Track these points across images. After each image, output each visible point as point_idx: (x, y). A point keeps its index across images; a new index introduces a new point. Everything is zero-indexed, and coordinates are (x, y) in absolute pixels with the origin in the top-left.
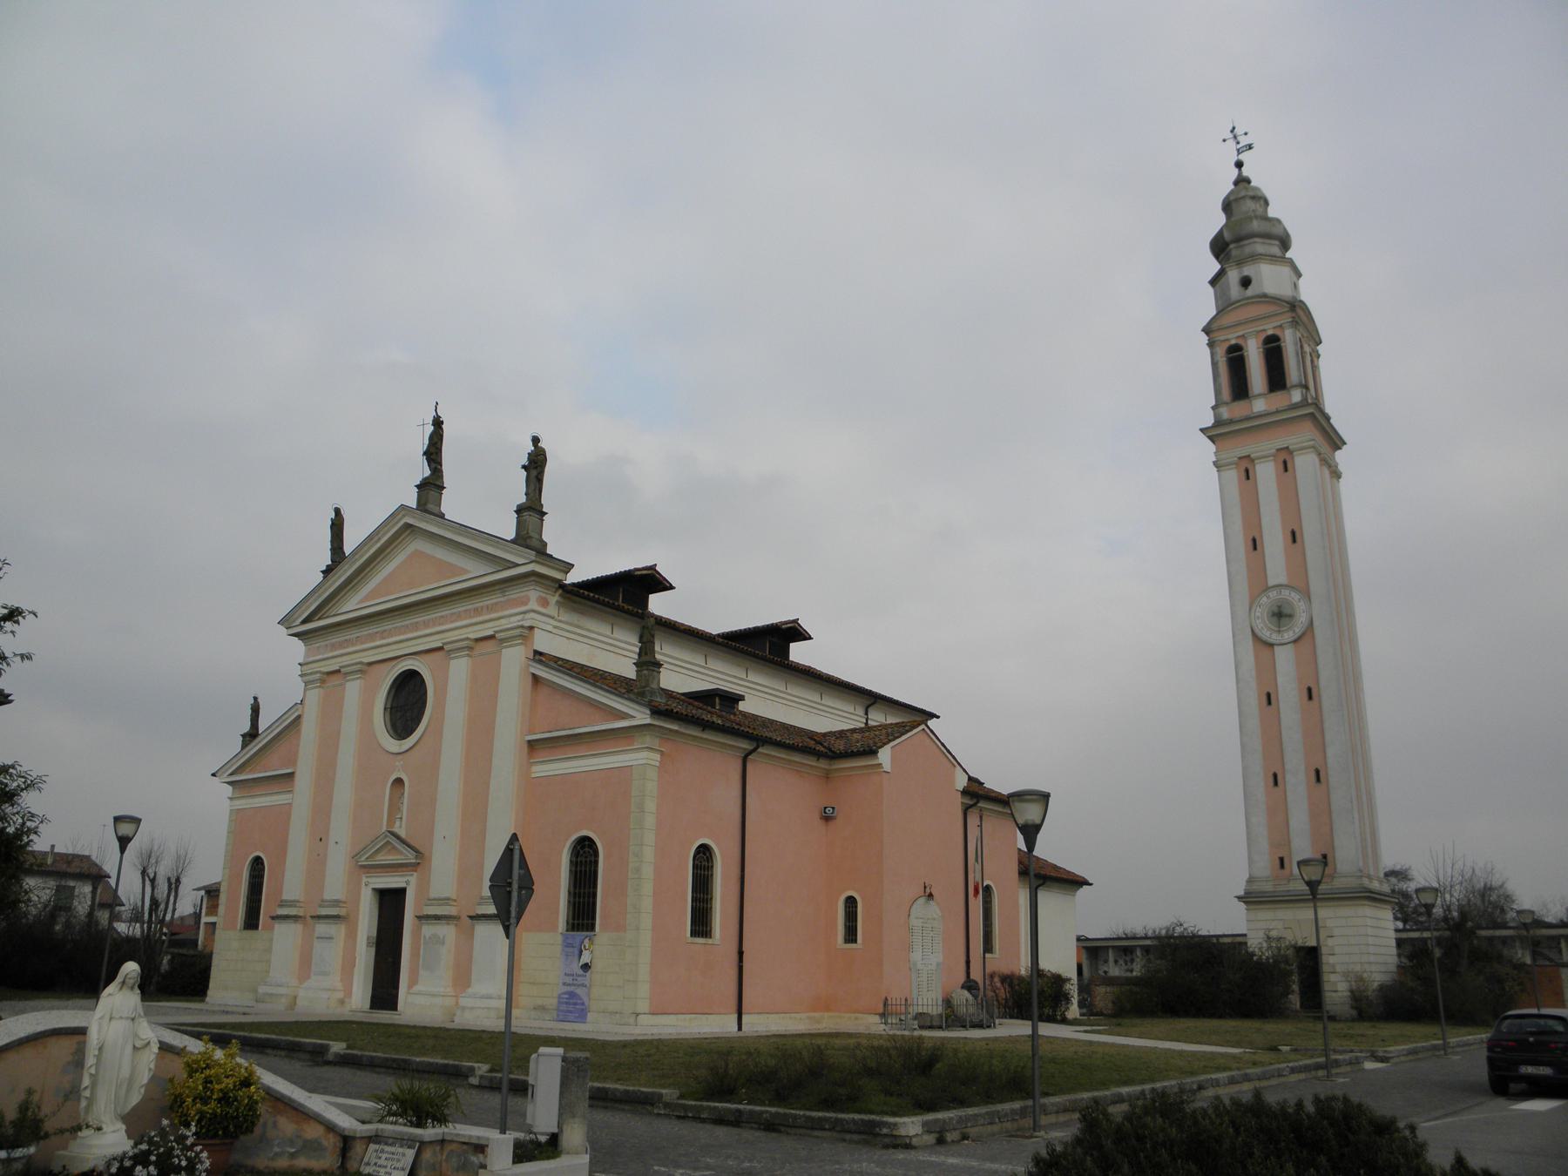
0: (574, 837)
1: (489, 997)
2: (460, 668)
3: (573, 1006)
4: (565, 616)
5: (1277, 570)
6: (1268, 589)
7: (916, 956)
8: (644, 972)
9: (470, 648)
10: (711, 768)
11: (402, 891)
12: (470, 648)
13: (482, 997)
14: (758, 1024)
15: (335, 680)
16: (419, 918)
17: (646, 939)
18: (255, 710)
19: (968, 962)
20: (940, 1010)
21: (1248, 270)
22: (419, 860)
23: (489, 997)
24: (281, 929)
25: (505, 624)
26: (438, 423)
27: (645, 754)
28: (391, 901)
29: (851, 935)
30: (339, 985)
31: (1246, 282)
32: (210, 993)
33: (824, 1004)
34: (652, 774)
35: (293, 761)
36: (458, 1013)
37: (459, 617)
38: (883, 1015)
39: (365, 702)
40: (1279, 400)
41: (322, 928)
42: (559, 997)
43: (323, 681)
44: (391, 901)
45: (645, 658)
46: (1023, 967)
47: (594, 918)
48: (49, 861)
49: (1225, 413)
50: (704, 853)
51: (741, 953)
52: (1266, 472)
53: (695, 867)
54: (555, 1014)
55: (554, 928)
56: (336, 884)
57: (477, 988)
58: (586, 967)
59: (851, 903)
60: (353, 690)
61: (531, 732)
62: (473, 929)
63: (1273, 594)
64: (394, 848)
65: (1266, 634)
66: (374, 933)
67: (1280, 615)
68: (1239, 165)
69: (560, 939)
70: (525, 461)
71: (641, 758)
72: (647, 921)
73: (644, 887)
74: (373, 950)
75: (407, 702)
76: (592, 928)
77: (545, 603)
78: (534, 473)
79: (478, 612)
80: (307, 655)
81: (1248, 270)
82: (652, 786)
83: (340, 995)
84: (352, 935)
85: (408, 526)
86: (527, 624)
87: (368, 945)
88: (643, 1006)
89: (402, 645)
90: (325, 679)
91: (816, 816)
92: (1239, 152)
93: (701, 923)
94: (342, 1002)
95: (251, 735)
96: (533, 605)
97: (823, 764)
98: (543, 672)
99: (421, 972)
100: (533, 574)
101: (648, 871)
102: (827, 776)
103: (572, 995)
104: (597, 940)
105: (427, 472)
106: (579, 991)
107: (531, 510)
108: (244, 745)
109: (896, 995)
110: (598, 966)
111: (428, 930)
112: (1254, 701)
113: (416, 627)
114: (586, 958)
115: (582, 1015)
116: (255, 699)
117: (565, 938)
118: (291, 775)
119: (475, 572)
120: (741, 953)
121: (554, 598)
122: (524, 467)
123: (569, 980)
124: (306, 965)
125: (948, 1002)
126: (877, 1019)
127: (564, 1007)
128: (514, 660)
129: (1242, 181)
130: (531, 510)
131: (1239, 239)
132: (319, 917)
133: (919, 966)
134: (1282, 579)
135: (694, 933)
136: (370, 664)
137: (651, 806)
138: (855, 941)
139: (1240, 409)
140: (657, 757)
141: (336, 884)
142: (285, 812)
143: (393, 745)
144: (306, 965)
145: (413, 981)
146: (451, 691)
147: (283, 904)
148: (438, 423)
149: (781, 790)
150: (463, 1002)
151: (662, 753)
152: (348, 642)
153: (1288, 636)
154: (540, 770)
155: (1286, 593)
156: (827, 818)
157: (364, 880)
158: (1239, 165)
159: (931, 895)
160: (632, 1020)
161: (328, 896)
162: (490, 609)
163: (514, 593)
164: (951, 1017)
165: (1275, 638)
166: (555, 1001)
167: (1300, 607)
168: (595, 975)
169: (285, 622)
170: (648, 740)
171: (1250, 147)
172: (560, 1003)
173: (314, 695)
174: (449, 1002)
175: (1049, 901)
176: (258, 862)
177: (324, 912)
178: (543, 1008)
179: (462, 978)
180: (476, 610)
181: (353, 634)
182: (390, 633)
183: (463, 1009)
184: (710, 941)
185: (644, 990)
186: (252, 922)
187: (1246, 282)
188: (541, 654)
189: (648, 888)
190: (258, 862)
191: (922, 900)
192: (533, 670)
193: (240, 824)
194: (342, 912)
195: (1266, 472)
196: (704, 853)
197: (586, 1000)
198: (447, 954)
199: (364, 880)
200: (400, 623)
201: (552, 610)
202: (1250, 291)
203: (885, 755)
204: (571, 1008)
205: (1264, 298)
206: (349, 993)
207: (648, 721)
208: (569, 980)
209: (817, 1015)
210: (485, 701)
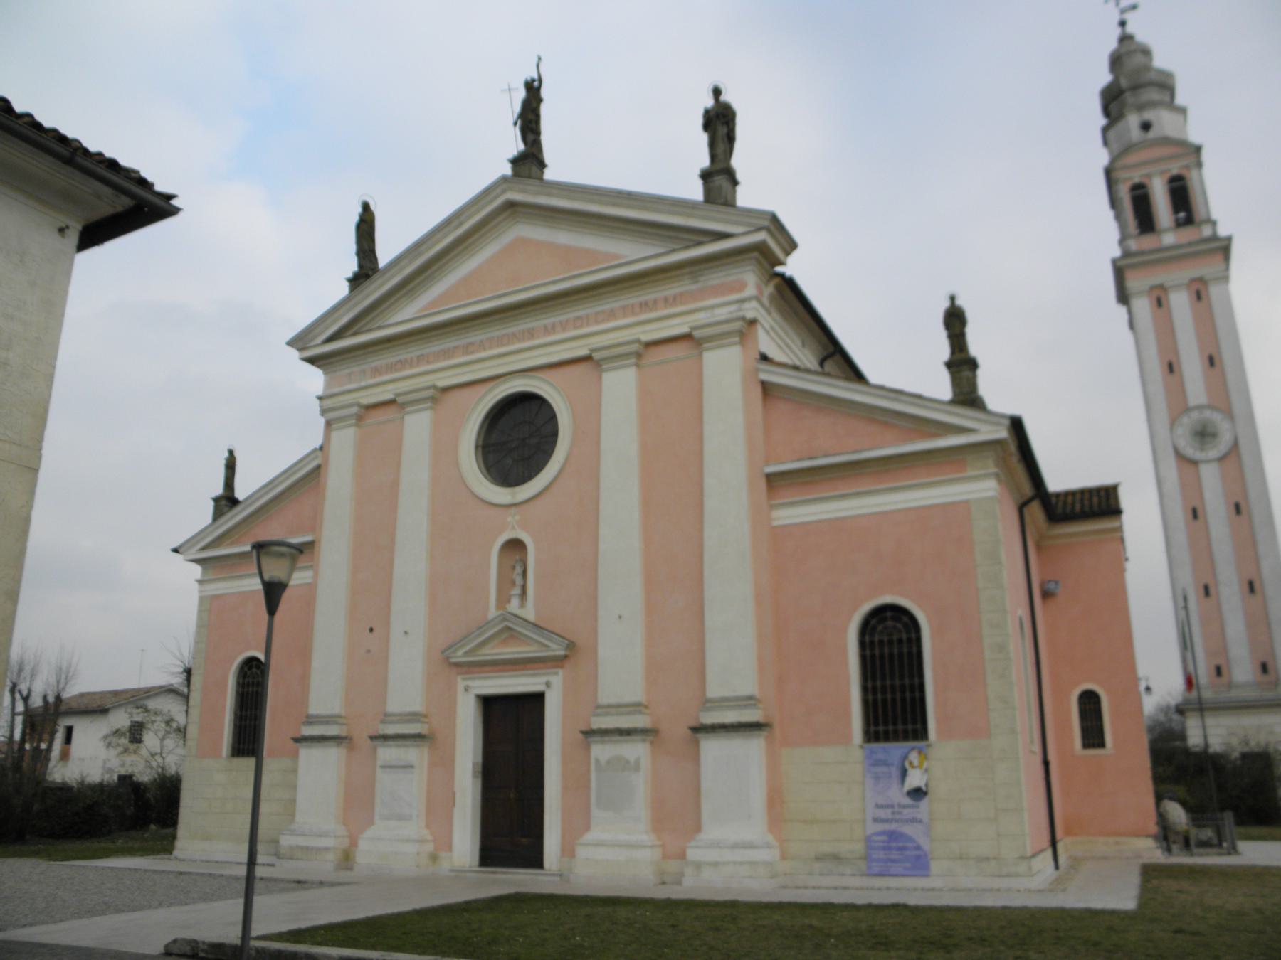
2: (620, 385)
5: (1196, 391)
6: (1187, 409)
9: (638, 355)
11: (536, 700)
13: (735, 846)
18: (231, 466)
19: (1046, 764)
21: (1149, 115)
22: (570, 653)
23: (750, 846)
24: (308, 755)
25: (701, 317)
31: (1146, 126)
37: (612, 315)
39: (437, 447)
40: (1188, 234)
41: (388, 753)
43: (359, 418)
45: (959, 356)
49: (1133, 245)
52: (1180, 302)
55: (847, 739)
56: (407, 686)
60: (417, 427)
63: (1195, 415)
65: (1190, 452)
66: (479, 759)
67: (1204, 434)
68: (1123, 24)
75: (518, 436)
79: (645, 306)
80: (328, 385)
81: (1149, 115)
84: (443, 763)
85: (511, 205)
89: (508, 362)
92: (1123, 11)
95: (227, 501)
99: (595, 812)
106: (908, 829)
108: (218, 514)
110: (940, 789)
112: (1179, 515)
113: (531, 334)
114: (915, 779)
116: (231, 452)
119: (634, 254)
123: (883, 814)
124: (359, 803)
126: (1150, 843)
128: (724, 371)
129: (1125, 39)
131: (1136, 88)
132: (385, 738)
134: (1203, 400)
136: (446, 390)
138: (1102, 744)
139: (1148, 242)
141: (407, 686)
143: (501, 495)
144: (359, 803)
145: (578, 822)
146: (608, 422)
152: (403, 364)
153: (1213, 453)
154: (790, 515)
155: (1208, 414)
158: (1123, 24)
161: (394, 706)
162: (675, 300)
163: (715, 278)
165: (1198, 455)
166: (859, 847)
167: (1223, 426)
169: (299, 342)
171: (1134, 7)
173: (345, 438)
177: (391, 730)
178: (836, 858)
181: (413, 351)
182: (482, 346)
183: (698, 866)
187: (1146, 126)
192: (764, 377)
195: (1180, 302)
200: (496, 331)
202: (1152, 134)
204: (895, 855)
205: (1166, 141)
206: (445, 842)
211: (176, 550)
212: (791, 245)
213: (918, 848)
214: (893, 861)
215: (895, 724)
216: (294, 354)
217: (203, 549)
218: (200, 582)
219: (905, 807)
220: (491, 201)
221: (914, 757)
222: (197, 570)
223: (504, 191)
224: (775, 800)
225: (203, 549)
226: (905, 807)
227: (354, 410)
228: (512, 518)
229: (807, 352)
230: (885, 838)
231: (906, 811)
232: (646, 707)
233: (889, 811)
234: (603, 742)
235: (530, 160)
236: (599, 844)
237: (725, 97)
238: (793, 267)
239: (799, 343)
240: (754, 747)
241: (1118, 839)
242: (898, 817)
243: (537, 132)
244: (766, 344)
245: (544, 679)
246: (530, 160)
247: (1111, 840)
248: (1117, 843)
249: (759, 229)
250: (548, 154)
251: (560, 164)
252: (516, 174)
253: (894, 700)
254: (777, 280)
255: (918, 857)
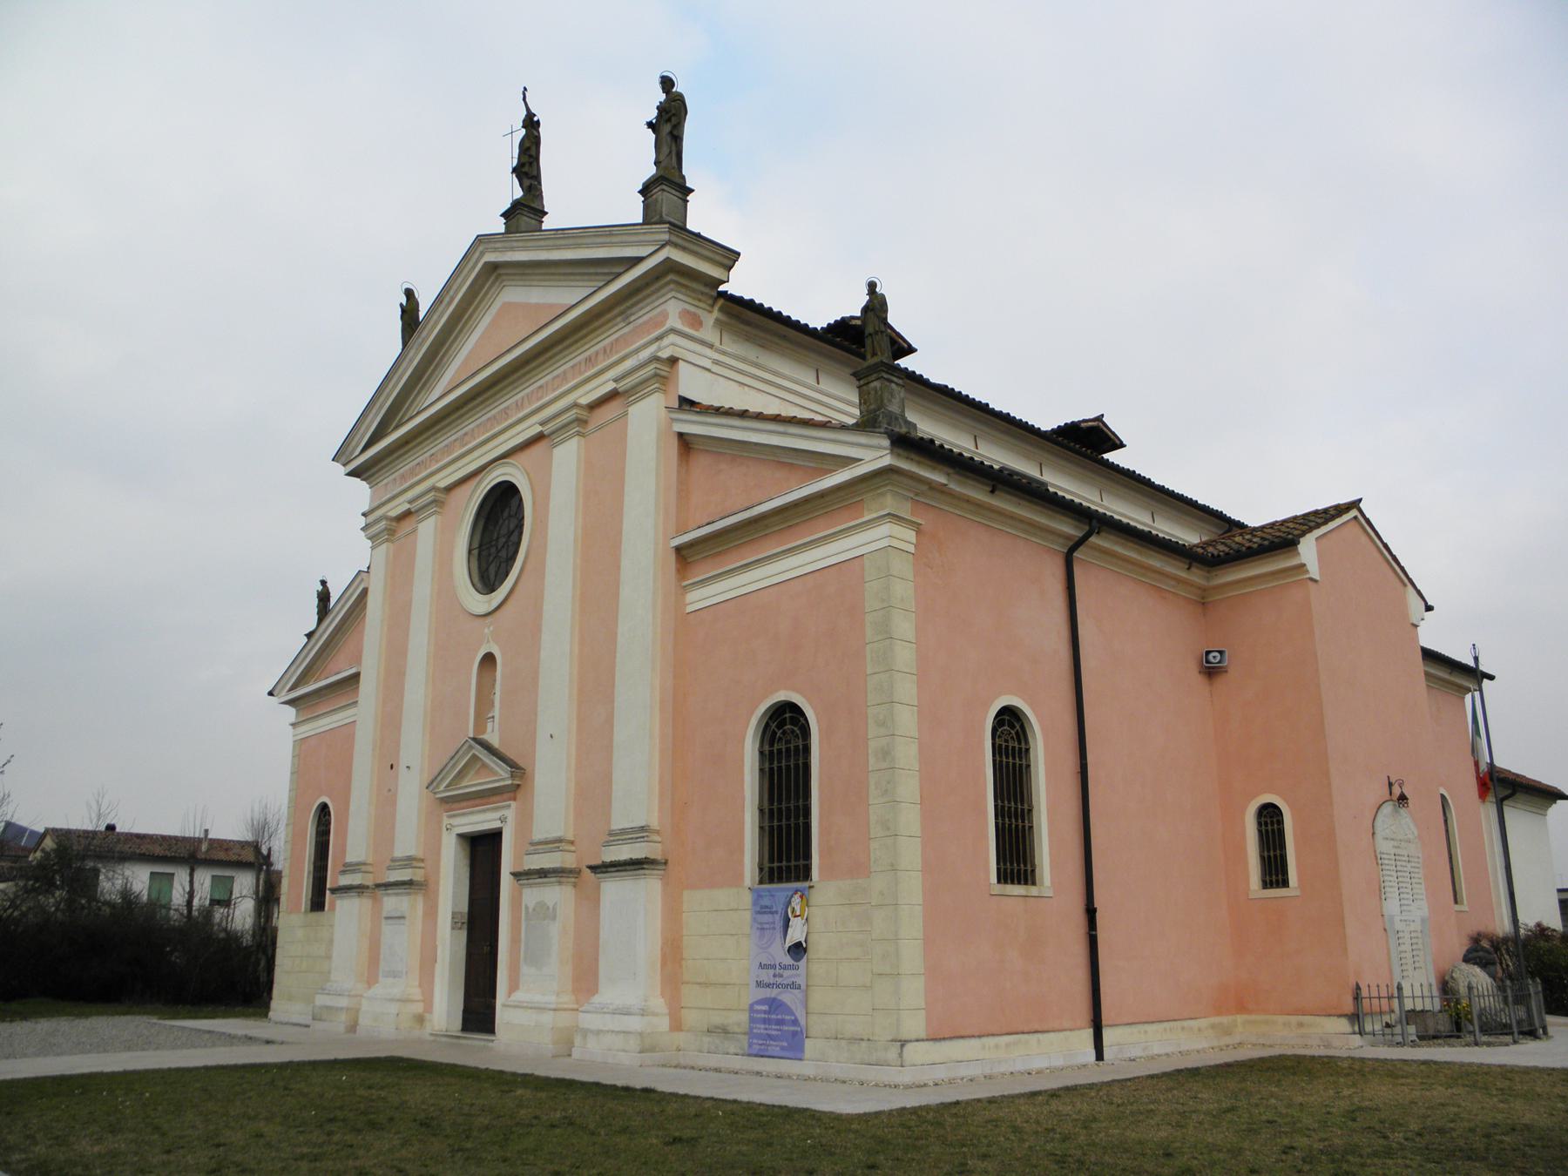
0: (763, 708)
1: (626, 1012)
2: (567, 456)
3: (776, 1027)
4: (731, 346)
7: (1392, 906)
8: (912, 954)
10: (1014, 578)
12: (582, 422)
14: (1140, 1046)
15: (406, 526)
16: (514, 874)
17: (912, 887)
20: (1437, 1002)
22: (517, 781)
23: (626, 1012)
26: (531, 123)
27: (886, 529)
28: (483, 850)
29: (1274, 872)
30: (416, 993)
32: (273, 1004)
33: (1237, 1000)
34: (902, 566)
35: (358, 659)
36: (578, 1040)
37: (564, 377)
38: (1355, 1017)
39: (446, 539)
41: (392, 903)
42: (751, 1009)
44: (483, 850)
46: (1503, 927)
47: (808, 855)
48: (204, 847)
50: (1010, 723)
51: (1091, 912)
53: (996, 749)
54: (744, 1040)
57: (608, 995)
58: (798, 950)
59: (1269, 817)
60: (427, 530)
61: (681, 531)
62: (598, 888)
64: (484, 765)
66: (464, 907)
69: (747, 898)
70: (652, 115)
71: (878, 539)
72: (911, 854)
73: (900, 796)
74: (463, 935)
75: (499, 525)
76: (805, 874)
77: (697, 323)
78: (667, 128)
82: (903, 590)
83: (418, 1008)
84: (431, 913)
85: (493, 268)
86: (665, 354)
87: (455, 926)
88: (915, 1025)
90: (387, 528)
91: (1192, 669)
93: (1015, 861)
94: (420, 1019)
96: (674, 321)
97: (1196, 576)
98: (694, 426)
100: (669, 267)
101: (907, 754)
102: (1203, 602)
103: (774, 1005)
104: (816, 897)
105: (519, 193)
106: (787, 997)
107: (667, 185)
109: (1371, 981)
110: (818, 948)
111: (534, 895)
114: (796, 933)
115: (794, 1044)
116: (323, 583)
117: (758, 896)
118: (356, 676)
120: (1091, 912)
121: (710, 318)
122: (650, 125)
123: (766, 976)
125: (1446, 988)
126: (1343, 1025)
127: (760, 1029)
128: (647, 420)
130: (667, 185)
133: (1399, 926)
135: (1004, 877)
136: (449, 489)
137: (904, 627)
138: (1285, 883)
140: (911, 535)
142: (346, 734)
143: (479, 603)
144: (372, 969)
145: (514, 987)
147: (349, 868)
148: (531, 123)
149: (1134, 624)
150: (589, 1021)
151: (918, 528)
154: (700, 598)
156: (1211, 671)
157: (446, 821)
159: (1403, 798)
160: (892, 1054)
163: (644, 314)
164: (1456, 1020)
166: (744, 1017)
168: (817, 965)
170: (890, 502)
172: (752, 1020)
174: (564, 1020)
175: (1518, 819)
176: (324, 809)
178: (724, 1031)
179: (585, 978)
180: (589, 360)
183: (585, 1033)
184: (1033, 890)
185: (913, 991)
186: (317, 904)
188: (692, 403)
189: (909, 788)
190: (324, 809)
191: (1388, 809)
193: (304, 751)
194: (418, 875)
196: (1010, 723)
197: (800, 1014)
198: (559, 937)
199: (446, 821)
201: (709, 333)
203: (1308, 549)
206: (429, 1006)
207: (887, 460)
208: (766, 976)
209: (1225, 1020)
210: (603, 498)
211: (271, 694)
212: (729, 257)
213: (795, 1022)
214: (770, 1037)
215: (789, 860)
216: (340, 470)
217: (292, 689)
218: (294, 725)
219: (785, 968)
220: (473, 268)
221: (796, 900)
222: (290, 713)
223: (482, 254)
224: (672, 952)
225: (292, 689)
226: (785, 968)
227: (383, 524)
228: (487, 628)
229: (827, 384)
230: (765, 1008)
231: (786, 973)
232: (572, 843)
233: (771, 972)
234: (560, 883)
235: (526, 211)
236: (601, 1010)
237: (679, 88)
238: (739, 284)
239: (810, 378)
240: (648, 888)
241: (1300, 1018)
242: (779, 980)
243: (537, 178)
244: (692, 383)
245: (497, 815)
246: (526, 211)
247: (1294, 1019)
248: (1301, 1025)
249: (663, 246)
250: (549, 200)
251: (560, 212)
252: (509, 230)
253: (788, 826)
254: (721, 302)
255: (794, 1034)
